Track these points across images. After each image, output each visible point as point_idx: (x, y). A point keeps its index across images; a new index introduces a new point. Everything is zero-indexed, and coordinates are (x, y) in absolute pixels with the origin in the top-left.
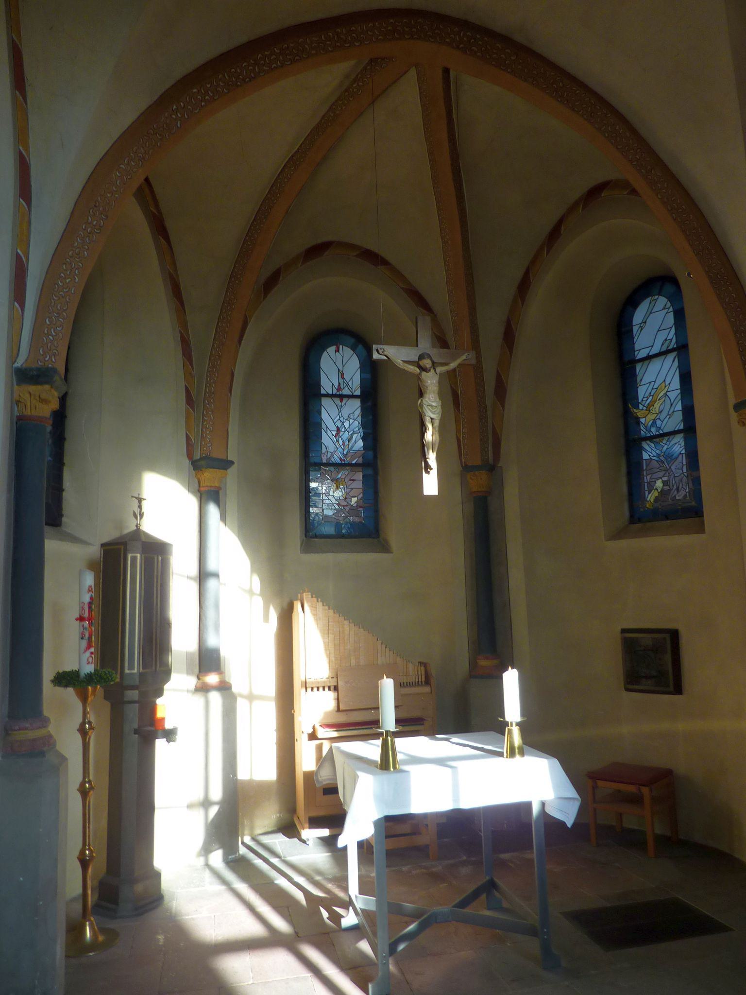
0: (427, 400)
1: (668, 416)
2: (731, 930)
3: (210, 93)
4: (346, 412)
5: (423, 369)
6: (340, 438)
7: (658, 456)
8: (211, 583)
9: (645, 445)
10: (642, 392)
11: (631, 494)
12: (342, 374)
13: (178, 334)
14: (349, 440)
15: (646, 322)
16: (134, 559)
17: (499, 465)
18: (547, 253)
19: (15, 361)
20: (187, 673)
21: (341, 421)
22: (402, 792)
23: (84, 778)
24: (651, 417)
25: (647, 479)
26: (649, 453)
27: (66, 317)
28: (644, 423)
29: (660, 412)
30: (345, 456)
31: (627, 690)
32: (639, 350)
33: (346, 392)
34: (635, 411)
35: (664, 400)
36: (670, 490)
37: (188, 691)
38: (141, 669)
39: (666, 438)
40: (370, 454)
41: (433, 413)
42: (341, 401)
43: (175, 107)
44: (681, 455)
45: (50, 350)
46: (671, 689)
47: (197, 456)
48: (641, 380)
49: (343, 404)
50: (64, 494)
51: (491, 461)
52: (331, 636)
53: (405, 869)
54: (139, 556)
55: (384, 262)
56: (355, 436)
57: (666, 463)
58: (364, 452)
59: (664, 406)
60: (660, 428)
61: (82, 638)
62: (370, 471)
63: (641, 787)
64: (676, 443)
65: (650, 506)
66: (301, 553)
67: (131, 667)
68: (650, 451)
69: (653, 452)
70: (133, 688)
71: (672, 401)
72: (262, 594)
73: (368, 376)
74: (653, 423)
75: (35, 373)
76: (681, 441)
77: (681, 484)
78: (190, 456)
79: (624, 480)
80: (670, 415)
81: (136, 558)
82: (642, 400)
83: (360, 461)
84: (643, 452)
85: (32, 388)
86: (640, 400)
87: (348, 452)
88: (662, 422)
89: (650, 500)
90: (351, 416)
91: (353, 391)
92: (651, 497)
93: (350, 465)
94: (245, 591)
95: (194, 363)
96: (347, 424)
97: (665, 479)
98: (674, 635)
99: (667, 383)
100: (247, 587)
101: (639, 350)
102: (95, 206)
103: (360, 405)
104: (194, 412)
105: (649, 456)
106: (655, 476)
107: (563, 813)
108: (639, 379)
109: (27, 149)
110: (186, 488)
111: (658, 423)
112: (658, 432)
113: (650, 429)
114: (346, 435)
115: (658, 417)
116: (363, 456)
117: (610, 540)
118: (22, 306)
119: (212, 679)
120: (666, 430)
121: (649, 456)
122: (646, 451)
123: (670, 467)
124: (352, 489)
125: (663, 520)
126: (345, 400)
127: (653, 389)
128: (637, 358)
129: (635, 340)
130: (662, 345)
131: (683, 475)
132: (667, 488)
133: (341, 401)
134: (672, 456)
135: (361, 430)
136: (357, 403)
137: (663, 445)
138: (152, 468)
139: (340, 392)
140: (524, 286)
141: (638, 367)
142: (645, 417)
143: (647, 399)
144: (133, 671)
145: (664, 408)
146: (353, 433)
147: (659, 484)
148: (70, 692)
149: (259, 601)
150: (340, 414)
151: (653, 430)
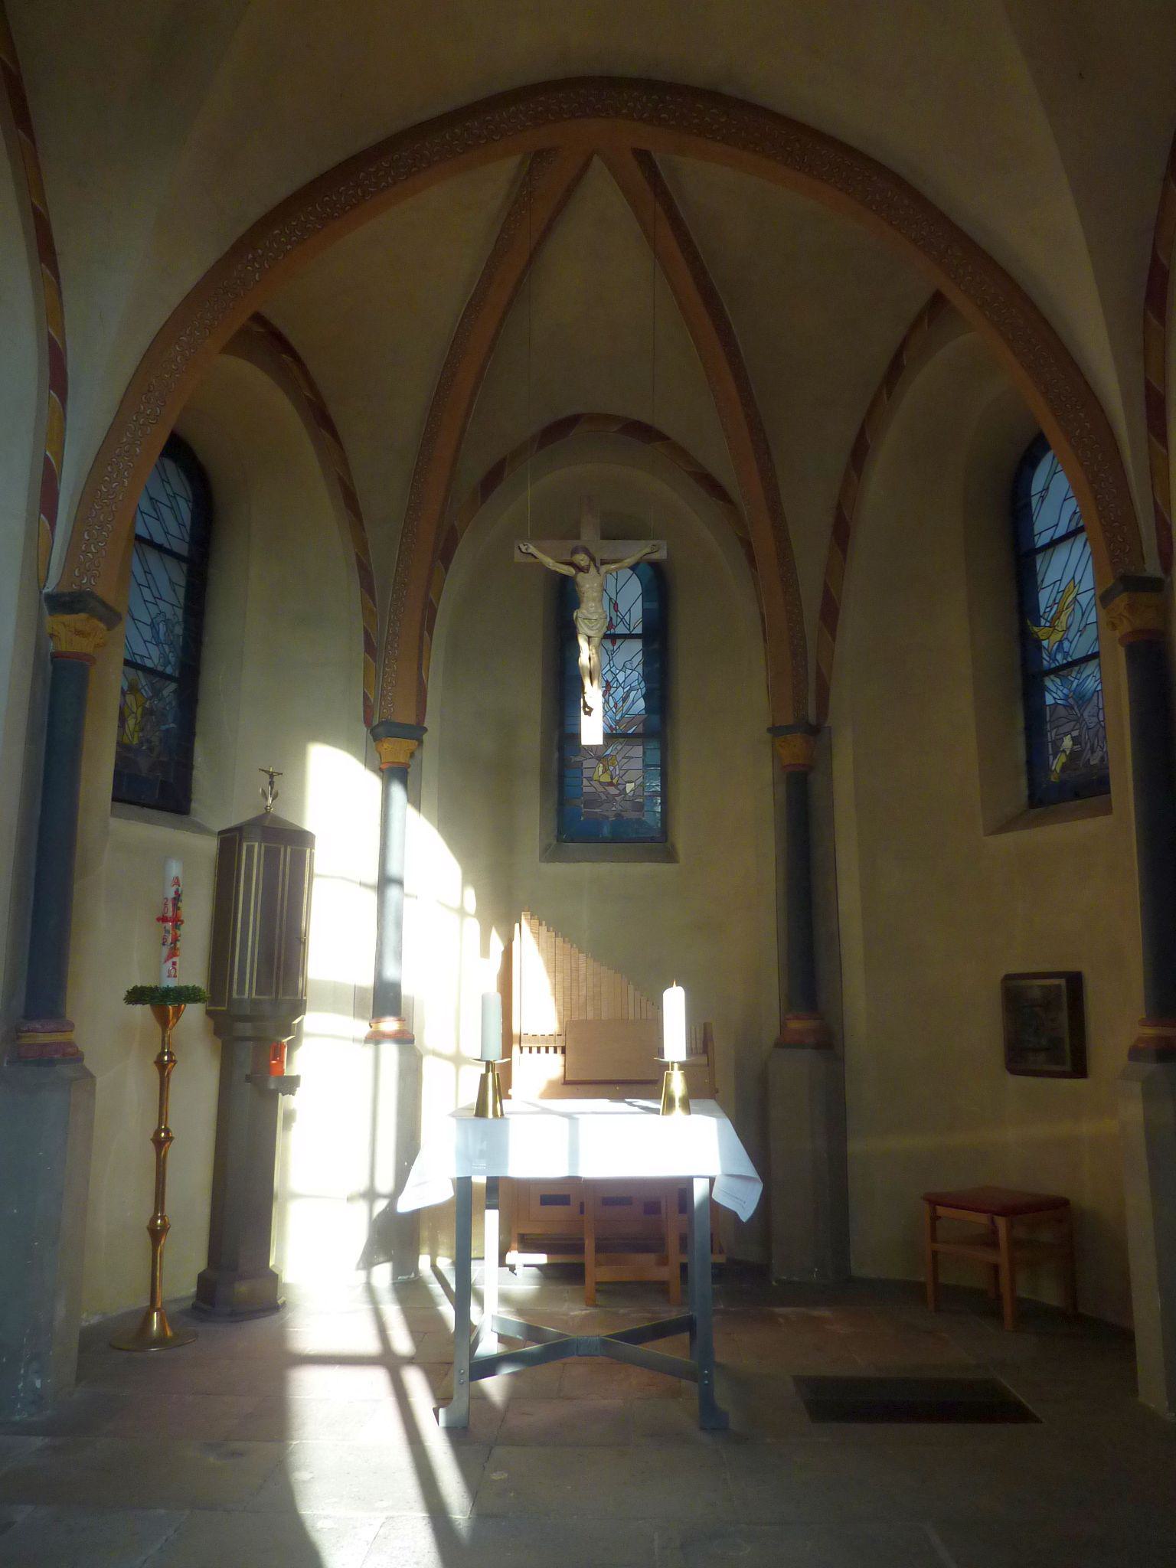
0: (584, 611)
1: (1079, 633)
2: (1038, 1421)
3: (297, 233)
4: (619, 659)
5: (579, 569)
6: (610, 697)
7: (1066, 699)
8: (393, 892)
9: (1048, 683)
10: (1044, 598)
11: (1029, 763)
12: (616, 605)
13: (354, 559)
14: (624, 700)
15: (1048, 488)
16: (250, 850)
17: (826, 725)
18: (888, 398)
19: (45, 586)
20: (354, 1015)
21: (612, 672)
22: (497, 1148)
23: (160, 1124)
24: (1057, 637)
25: (1051, 735)
26: (1055, 695)
27: (110, 529)
28: (1046, 647)
29: (1068, 628)
30: (617, 722)
31: (1013, 1071)
32: (1040, 533)
33: (621, 629)
34: (1036, 629)
35: (1073, 609)
36: (1082, 751)
37: (354, 1040)
38: (254, 994)
39: (1077, 668)
40: (655, 719)
41: (590, 628)
42: (614, 644)
43: (250, 256)
44: (1096, 694)
45: (88, 571)
46: (1068, 1068)
47: (376, 722)
48: (1043, 581)
49: (615, 648)
50: (195, 772)
51: (812, 718)
52: (559, 976)
53: (622, 1311)
54: (257, 845)
55: (661, 437)
56: (633, 693)
57: (1075, 708)
58: (646, 716)
59: (1073, 619)
60: (1068, 653)
61: (164, 944)
62: (654, 744)
63: (995, 1217)
64: (1089, 676)
65: (1055, 779)
66: (541, 861)
67: (241, 991)
68: (1055, 691)
69: (1059, 693)
70: (247, 1019)
71: (1084, 607)
72: (478, 915)
73: (654, 605)
74: (1059, 646)
75: (67, 599)
76: (1097, 670)
77: (1096, 741)
78: (367, 721)
79: (1020, 742)
80: (1081, 632)
81: (253, 846)
82: (1045, 612)
83: (640, 730)
84: (1046, 693)
85: (68, 618)
86: (1041, 614)
87: (622, 717)
88: (1071, 643)
89: (1055, 769)
90: (628, 665)
91: (631, 629)
92: (1057, 764)
93: (625, 735)
94: (452, 909)
95: (377, 597)
96: (621, 677)
97: (1075, 733)
98: (1075, 981)
99: (1077, 581)
100: (457, 904)
101: (1040, 533)
102: (149, 391)
103: (641, 647)
104: (375, 662)
105: (1055, 698)
106: (1062, 730)
107: (736, 1200)
108: (1039, 579)
109: (62, 333)
110: (361, 761)
111: (1066, 644)
112: (1066, 659)
113: (1055, 654)
114: (620, 692)
115: (1065, 637)
116: (644, 722)
117: (993, 833)
118: (52, 521)
119: (389, 1025)
120: (1076, 656)
121: (1055, 698)
122: (1050, 691)
123: (1082, 715)
124: (627, 770)
125: (1072, 800)
126: (619, 642)
127: (1058, 592)
128: (1037, 547)
129: (1034, 518)
130: (1070, 521)
131: (1099, 726)
132: (1077, 748)
133: (614, 644)
134: (1084, 696)
135: (643, 684)
136: (637, 645)
137: (1073, 679)
138: (316, 738)
139: (612, 631)
140: (859, 454)
141: (1039, 559)
142: (1048, 638)
143: (1051, 609)
144: (243, 997)
145: (1072, 622)
146: (631, 689)
147: (1067, 742)
148: (142, 1012)
149: (473, 926)
150: (611, 662)
151: (1059, 657)
